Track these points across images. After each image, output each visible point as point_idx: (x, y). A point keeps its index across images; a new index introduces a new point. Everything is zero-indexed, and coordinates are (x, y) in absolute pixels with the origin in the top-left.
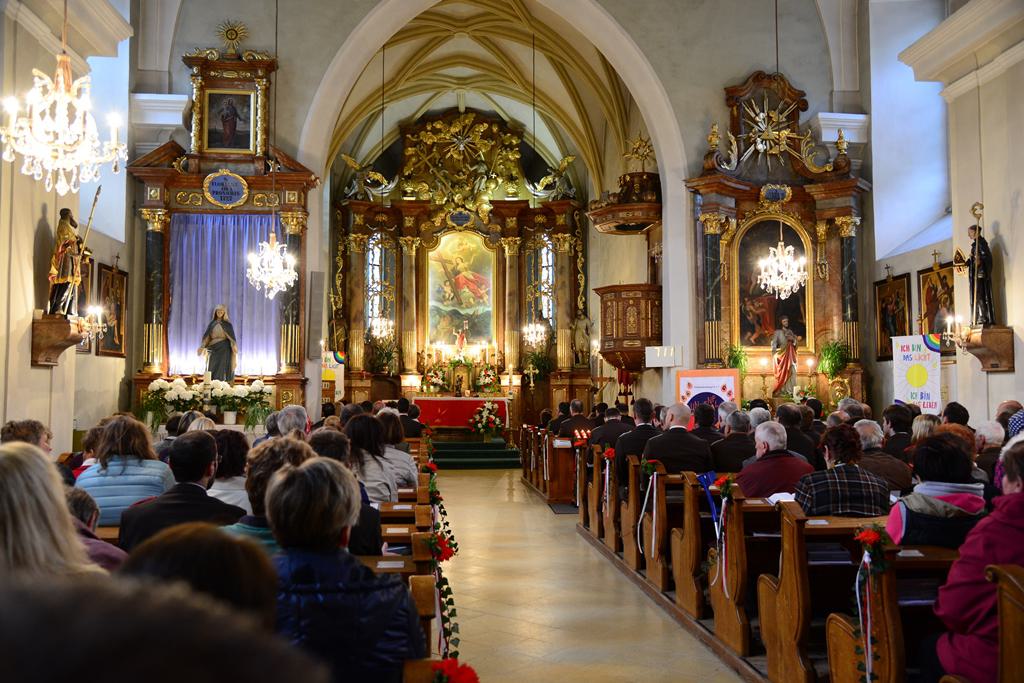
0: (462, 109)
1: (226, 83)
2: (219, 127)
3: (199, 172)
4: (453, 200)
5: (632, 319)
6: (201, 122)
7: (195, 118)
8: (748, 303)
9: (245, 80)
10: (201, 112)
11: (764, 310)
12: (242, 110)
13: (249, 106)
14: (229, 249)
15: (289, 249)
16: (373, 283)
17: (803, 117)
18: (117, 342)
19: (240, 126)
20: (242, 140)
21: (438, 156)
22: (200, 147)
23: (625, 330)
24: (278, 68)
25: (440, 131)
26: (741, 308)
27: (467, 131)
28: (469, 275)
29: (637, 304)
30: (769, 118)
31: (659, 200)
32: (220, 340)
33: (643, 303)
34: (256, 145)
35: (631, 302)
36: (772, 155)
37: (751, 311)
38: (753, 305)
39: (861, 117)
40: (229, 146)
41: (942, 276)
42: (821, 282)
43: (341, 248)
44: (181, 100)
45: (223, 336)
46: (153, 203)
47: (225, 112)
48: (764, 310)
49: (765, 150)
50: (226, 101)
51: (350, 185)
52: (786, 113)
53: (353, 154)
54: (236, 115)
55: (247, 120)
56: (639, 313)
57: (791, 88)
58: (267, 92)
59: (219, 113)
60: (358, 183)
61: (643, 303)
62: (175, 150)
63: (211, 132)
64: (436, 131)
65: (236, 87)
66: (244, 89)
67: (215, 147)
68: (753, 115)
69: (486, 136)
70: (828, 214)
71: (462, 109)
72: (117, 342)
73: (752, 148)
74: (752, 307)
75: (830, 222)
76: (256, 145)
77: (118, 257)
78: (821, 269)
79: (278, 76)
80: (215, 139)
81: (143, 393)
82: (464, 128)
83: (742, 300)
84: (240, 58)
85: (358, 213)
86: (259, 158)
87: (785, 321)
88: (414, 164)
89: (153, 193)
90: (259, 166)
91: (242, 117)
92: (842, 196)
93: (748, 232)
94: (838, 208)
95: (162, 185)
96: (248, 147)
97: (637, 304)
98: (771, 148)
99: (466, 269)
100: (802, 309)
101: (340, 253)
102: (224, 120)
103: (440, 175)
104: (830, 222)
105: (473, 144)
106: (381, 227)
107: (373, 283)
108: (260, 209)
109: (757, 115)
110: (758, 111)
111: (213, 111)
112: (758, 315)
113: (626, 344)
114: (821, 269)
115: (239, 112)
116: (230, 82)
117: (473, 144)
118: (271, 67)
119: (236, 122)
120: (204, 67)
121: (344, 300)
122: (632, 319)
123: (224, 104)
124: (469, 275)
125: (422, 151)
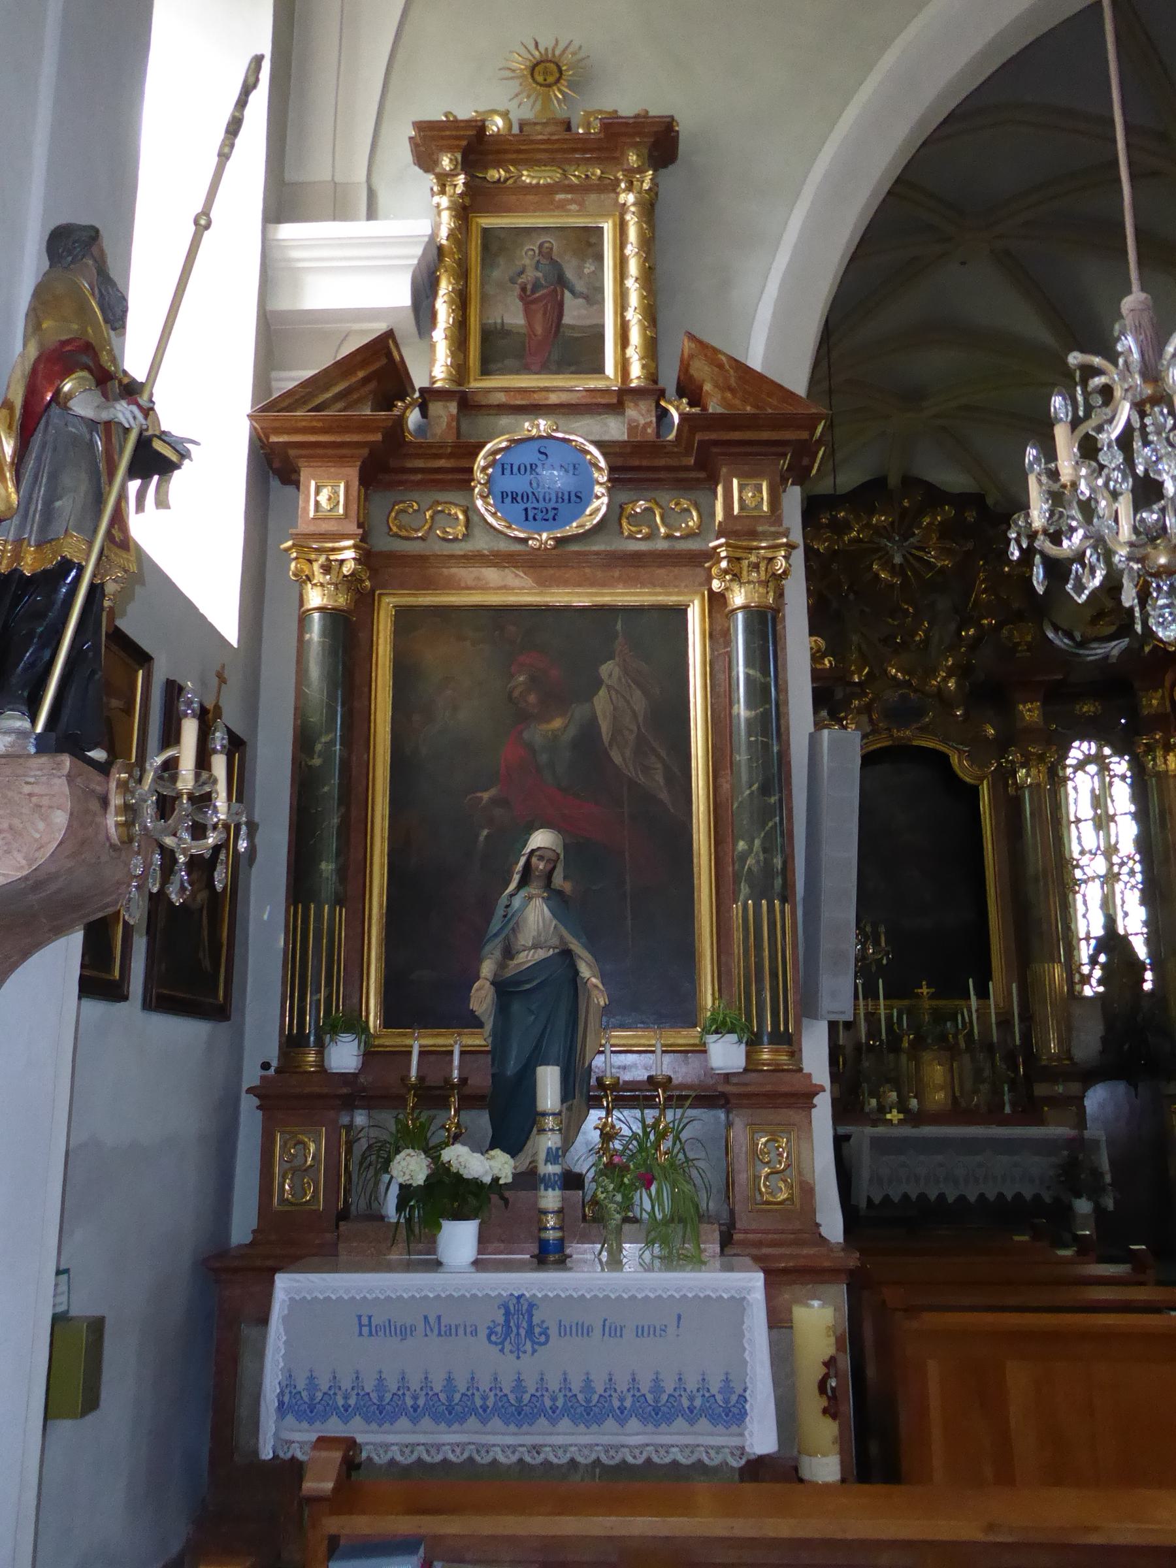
0: (893, 481)
1: (530, 198)
6: (461, 302)
7: (445, 287)
10: (462, 274)
12: (580, 268)
13: (600, 258)
15: (1142, 890)
16: (1082, 853)
18: (207, 964)
19: (574, 313)
20: (584, 352)
22: (460, 370)
24: (672, 117)
27: (905, 523)
32: (541, 954)
34: (624, 359)
40: (545, 368)
45: (555, 941)
46: (325, 527)
47: (531, 275)
50: (531, 246)
54: (562, 282)
55: (594, 296)
58: (649, 208)
59: (513, 281)
62: (377, 367)
63: (487, 335)
65: (562, 207)
66: (583, 211)
67: (504, 372)
69: (946, 531)
72: (207, 964)
76: (624, 359)
77: (222, 679)
86: (638, 393)
91: (580, 286)
95: (353, 473)
96: (599, 369)
102: (527, 298)
107: (1082, 853)
111: (496, 274)
115: (570, 274)
116: (544, 195)
118: (661, 142)
119: (561, 305)
120: (468, 151)
123: (526, 256)
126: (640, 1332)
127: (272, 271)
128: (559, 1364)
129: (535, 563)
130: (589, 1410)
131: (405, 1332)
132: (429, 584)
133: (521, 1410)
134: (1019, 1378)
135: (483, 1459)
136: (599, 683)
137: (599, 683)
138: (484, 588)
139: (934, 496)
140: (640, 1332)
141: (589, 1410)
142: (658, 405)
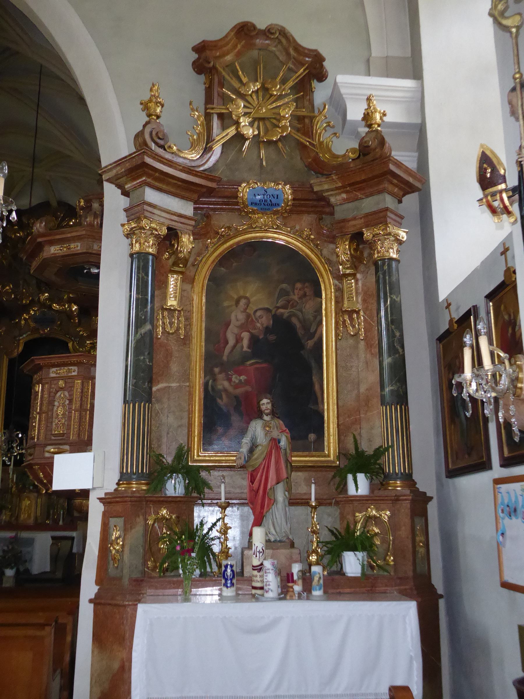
0: (54, 203)
5: (60, 411)
8: (221, 377)
14: (333, 411)
23: (48, 429)
26: (206, 385)
29: (69, 388)
35: (61, 383)
37: (226, 390)
38: (230, 380)
39: (409, 83)
41: (503, 256)
42: (351, 341)
48: (248, 388)
52: (290, 83)
57: (298, 48)
70: (352, 227)
74: (226, 384)
75: (357, 238)
78: (351, 319)
81: (342, 466)
83: (208, 371)
87: (266, 404)
92: (372, 195)
94: (367, 215)
98: (267, 131)
100: (317, 387)
104: (357, 238)
110: (245, 80)
112: (236, 397)
114: (351, 319)
122: (60, 411)
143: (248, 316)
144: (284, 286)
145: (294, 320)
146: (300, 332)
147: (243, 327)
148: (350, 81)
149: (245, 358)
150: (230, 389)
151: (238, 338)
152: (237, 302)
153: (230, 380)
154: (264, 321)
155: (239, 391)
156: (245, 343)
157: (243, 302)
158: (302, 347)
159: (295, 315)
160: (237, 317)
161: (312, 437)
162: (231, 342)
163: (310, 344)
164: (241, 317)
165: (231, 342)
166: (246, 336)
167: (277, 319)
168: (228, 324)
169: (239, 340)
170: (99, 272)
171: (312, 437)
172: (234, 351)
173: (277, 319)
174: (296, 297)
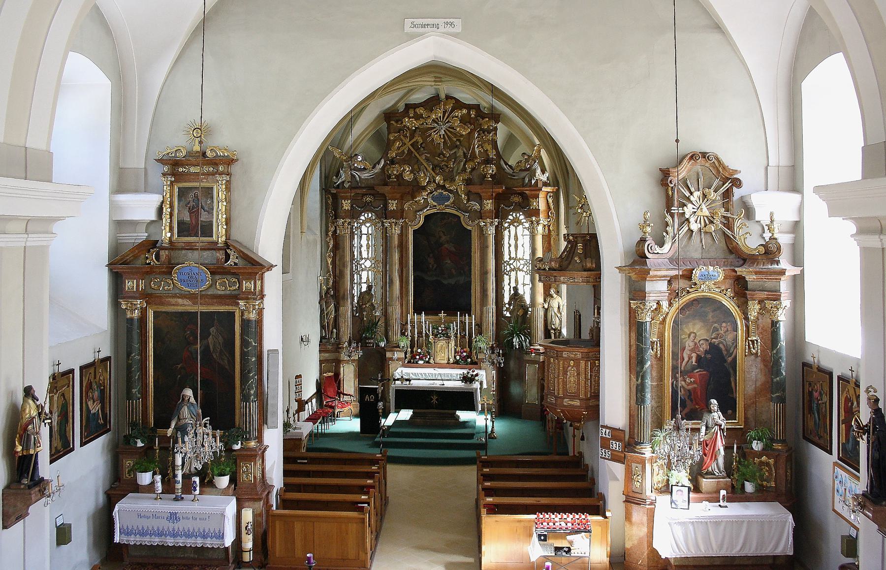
0: (443, 96)
2: (187, 218)
3: (170, 263)
4: (434, 181)
9: (209, 174)
10: (172, 207)
11: (695, 386)
17: (737, 193)
19: (204, 217)
20: (207, 230)
21: (421, 141)
25: (421, 116)
26: (672, 384)
28: (451, 247)
29: (577, 365)
30: (705, 196)
31: (598, 268)
33: (583, 363)
36: (706, 233)
37: (682, 387)
38: (685, 381)
43: (332, 229)
44: (155, 199)
47: (192, 204)
48: (695, 386)
49: (700, 230)
51: (337, 174)
53: (339, 146)
55: (210, 211)
56: (578, 374)
58: (228, 189)
60: (345, 172)
61: (583, 363)
62: (151, 245)
63: (180, 223)
64: (418, 117)
68: (687, 194)
69: (464, 121)
71: (443, 96)
73: (685, 229)
79: (235, 169)
80: (184, 229)
82: (444, 113)
83: (674, 377)
84: (204, 154)
85: (346, 198)
86: (220, 249)
88: (399, 148)
89: (130, 284)
90: (221, 255)
93: (682, 310)
97: (577, 365)
99: (448, 242)
101: (330, 234)
103: (422, 159)
105: (453, 128)
106: (366, 208)
108: (223, 293)
109: (691, 193)
110: (693, 190)
112: (689, 390)
113: (566, 402)
117: (453, 128)
120: (174, 166)
121: (335, 277)
123: (191, 195)
124: (451, 247)
125: (406, 136)
126: (200, 519)
127: (114, 207)
128: (180, 526)
129: (192, 297)
130: (188, 535)
131: (148, 518)
132: (162, 304)
133: (174, 535)
134: (298, 527)
135: (144, 544)
136: (210, 334)
137: (210, 334)
138: (177, 305)
139: (459, 105)
140: (200, 519)
141: (188, 535)
142: (226, 252)
143: (696, 344)
144: (716, 325)
145: (721, 346)
146: (725, 353)
147: (693, 351)
148: (354, 470)
149: (694, 368)
150: (685, 386)
151: (689, 357)
152: (689, 335)
153: (685, 381)
154: (704, 347)
155: (690, 387)
156: (694, 359)
157: (693, 335)
158: (725, 361)
159: (722, 343)
160: (689, 344)
161: (730, 412)
162: (686, 359)
163: (730, 359)
164: (692, 344)
165: (686, 359)
166: (694, 355)
167: (711, 345)
168: (684, 349)
169: (690, 358)
170: (802, 272)
171: (730, 412)
172: (184, 252)
173: (711, 345)
174: (722, 332)
